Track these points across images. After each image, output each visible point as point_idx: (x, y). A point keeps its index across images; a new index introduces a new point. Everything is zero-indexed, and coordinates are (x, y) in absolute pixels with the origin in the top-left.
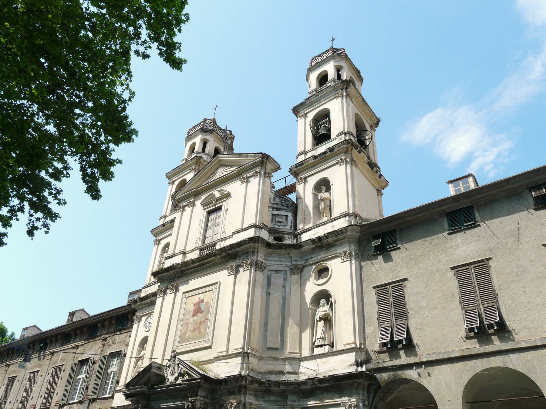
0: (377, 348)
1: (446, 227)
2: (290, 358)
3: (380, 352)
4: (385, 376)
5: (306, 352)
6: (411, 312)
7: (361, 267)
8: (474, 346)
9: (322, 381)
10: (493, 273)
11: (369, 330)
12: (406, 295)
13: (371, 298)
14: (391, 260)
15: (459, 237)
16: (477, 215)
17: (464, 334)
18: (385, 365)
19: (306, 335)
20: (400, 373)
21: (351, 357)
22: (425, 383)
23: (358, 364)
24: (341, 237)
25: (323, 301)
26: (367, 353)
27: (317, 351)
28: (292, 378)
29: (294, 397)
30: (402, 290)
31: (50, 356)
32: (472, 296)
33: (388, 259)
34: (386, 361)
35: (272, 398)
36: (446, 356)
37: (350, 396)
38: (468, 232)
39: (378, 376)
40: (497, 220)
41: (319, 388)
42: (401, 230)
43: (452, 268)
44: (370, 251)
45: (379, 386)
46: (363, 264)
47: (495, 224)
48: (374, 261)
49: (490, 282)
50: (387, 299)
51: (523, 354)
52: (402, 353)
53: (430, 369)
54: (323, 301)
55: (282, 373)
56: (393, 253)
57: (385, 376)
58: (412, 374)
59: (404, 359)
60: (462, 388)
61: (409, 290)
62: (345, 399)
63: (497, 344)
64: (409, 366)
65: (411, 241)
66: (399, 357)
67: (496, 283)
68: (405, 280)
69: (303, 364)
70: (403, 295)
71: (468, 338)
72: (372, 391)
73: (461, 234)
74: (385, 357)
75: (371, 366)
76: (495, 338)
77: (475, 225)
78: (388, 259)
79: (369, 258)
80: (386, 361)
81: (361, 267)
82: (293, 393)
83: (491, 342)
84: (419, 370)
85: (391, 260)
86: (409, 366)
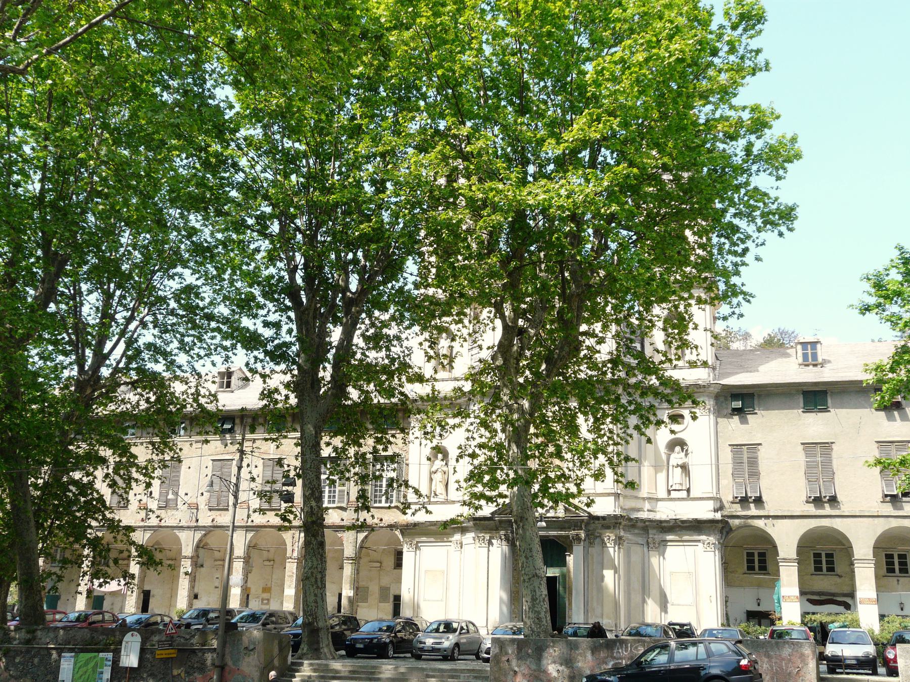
0: (731, 499)
1: (802, 405)
2: (650, 498)
3: (732, 503)
4: (737, 522)
5: (662, 494)
6: (762, 474)
7: (717, 423)
8: (811, 509)
9: (683, 522)
10: (834, 454)
11: (723, 482)
12: (759, 458)
13: (727, 456)
14: (747, 423)
15: (811, 416)
16: (829, 401)
17: (805, 499)
18: (738, 514)
19: (662, 476)
20: (749, 521)
21: (711, 505)
22: (770, 530)
23: (716, 511)
24: (701, 390)
25: (678, 449)
26: (721, 501)
27: (674, 494)
28: (651, 516)
29: (654, 531)
30: (755, 453)
31: (199, 445)
32: (815, 471)
33: (744, 421)
34: (737, 510)
35: (636, 531)
36: (789, 514)
37: (709, 535)
38: (820, 414)
39: (731, 521)
40: (844, 411)
41: (679, 526)
42: (759, 396)
43: (802, 444)
44: (727, 408)
45: (731, 529)
46: (719, 420)
47: (843, 413)
48: (730, 420)
49: (831, 462)
50: (742, 458)
51: (845, 519)
52: (752, 505)
53: (775, 521)
54: (678, 449)
55: (639, 510)
56: (749, 417)
57: (737, 522)
58: (760, 523)
59: (753, 511)
60: (798, 538)
61: (763, 455)
62: (703, 537)
63: (827, 510)
64: (759, 517)
65: (767, 409)
66: (749, 509)
67: (835, 464)
68: (760, 444)
69: (660, 503)
70: (756, 458)
71: (807, 502)
72: (725, 533)
73: (813, 415)
74: (737, 507)
75: (725, 513)
76: (827, 505)
77: (826, 410)
78: (744, 421)
79: (725, 416)
80: (737, 510)
81: (717, 423)
82: (654, 528)
83: (749, 509)
84: (766, 521)
85: (747, 423)
86: (759, 517)
